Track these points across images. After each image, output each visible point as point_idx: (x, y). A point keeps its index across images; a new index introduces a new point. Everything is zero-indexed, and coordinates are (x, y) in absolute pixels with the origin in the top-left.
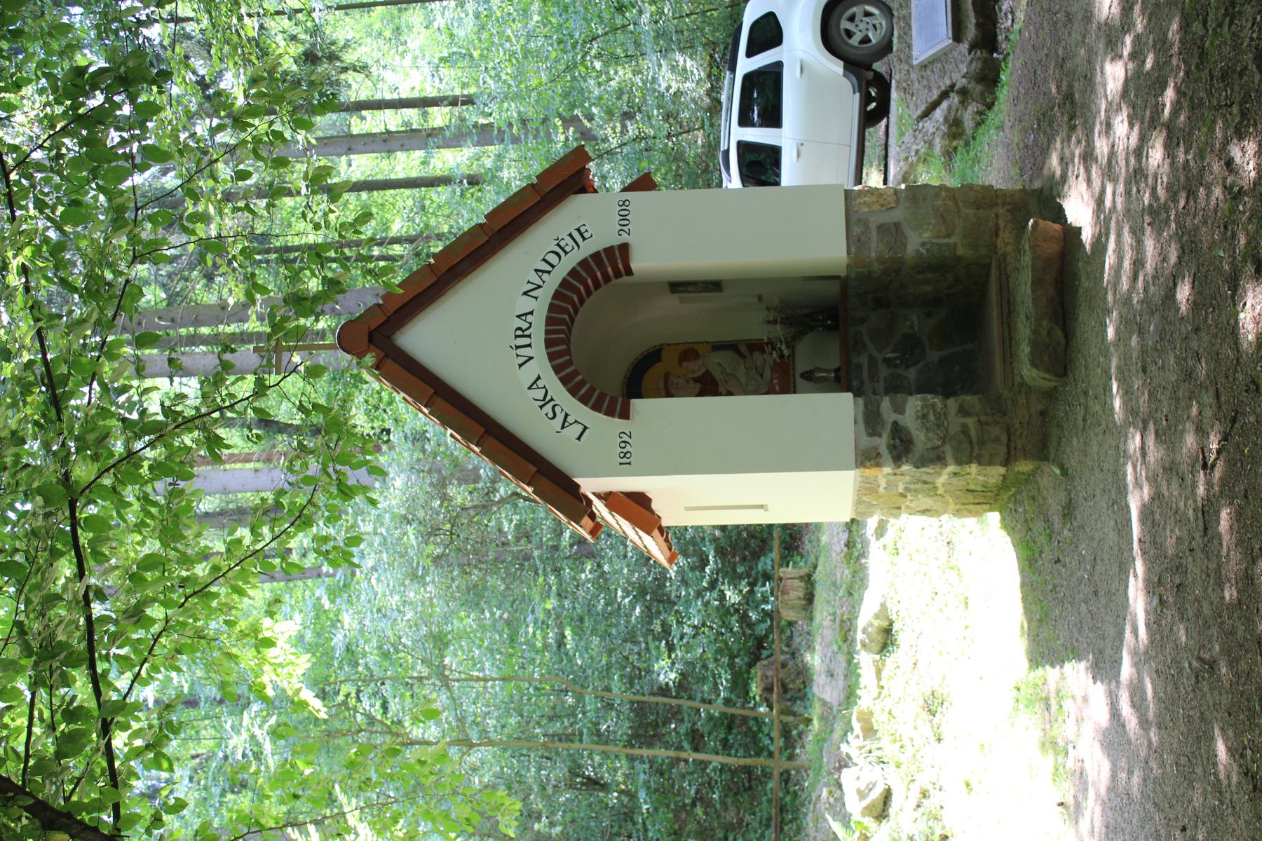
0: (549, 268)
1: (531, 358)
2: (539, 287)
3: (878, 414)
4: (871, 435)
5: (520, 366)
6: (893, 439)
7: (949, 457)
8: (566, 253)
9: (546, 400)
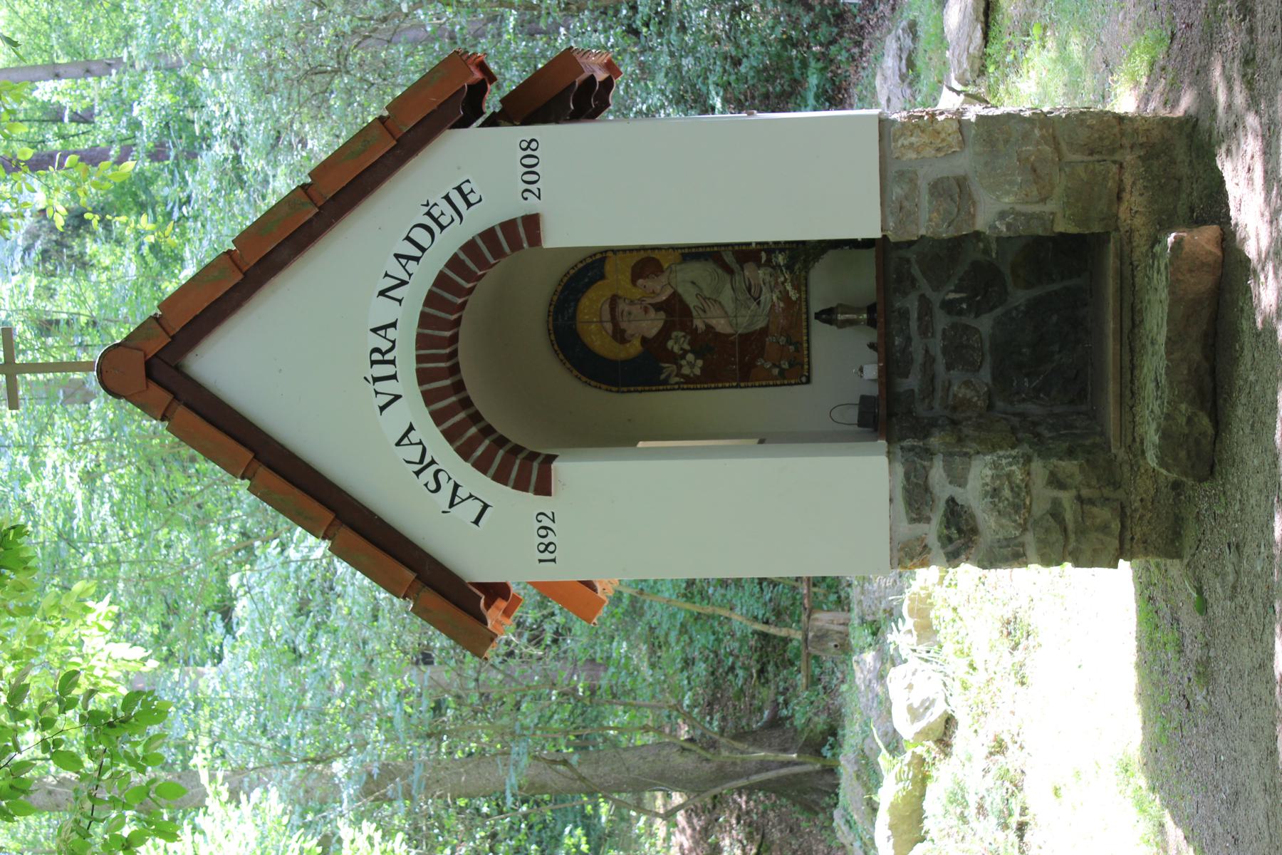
0: (417, 253)
1: (397, 397)
2: (403, 283)
3: (927, 489)
4: (912, 521)
5: (382, 408)
6: (948, 527)
7: (1031, 551)
8: (442, 228)
9: (424, 463)
